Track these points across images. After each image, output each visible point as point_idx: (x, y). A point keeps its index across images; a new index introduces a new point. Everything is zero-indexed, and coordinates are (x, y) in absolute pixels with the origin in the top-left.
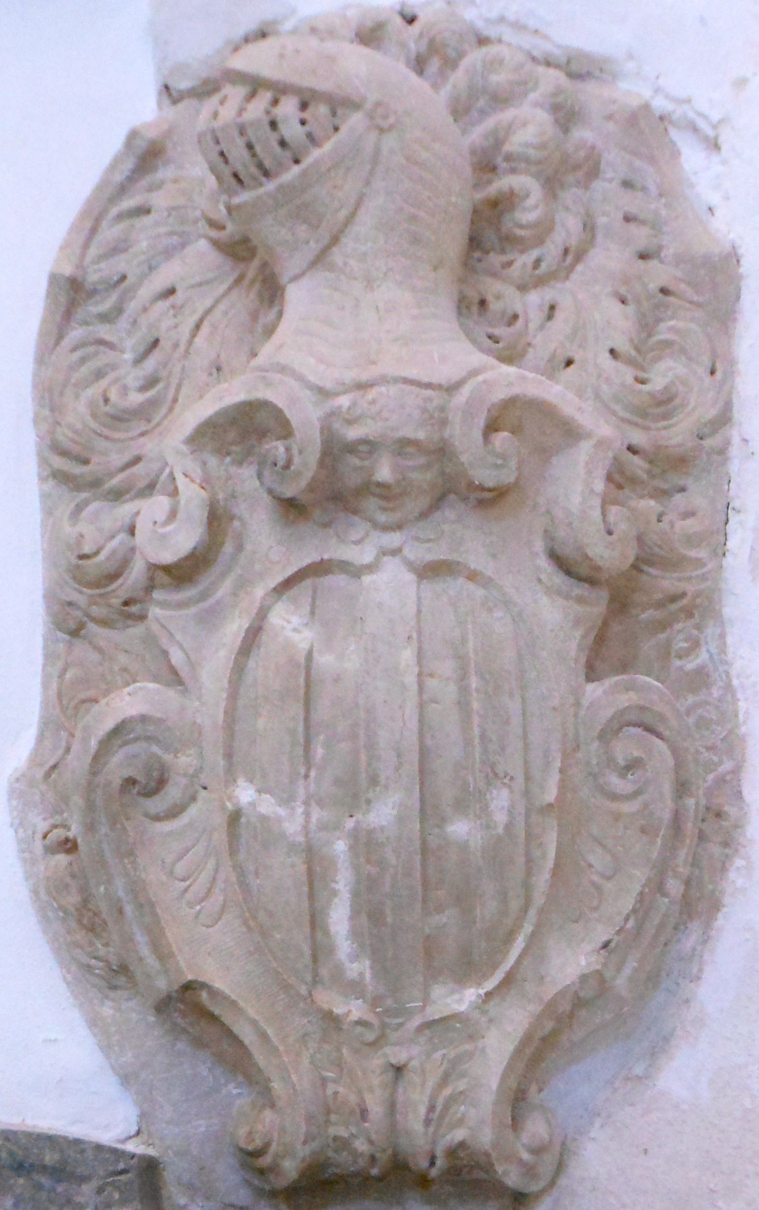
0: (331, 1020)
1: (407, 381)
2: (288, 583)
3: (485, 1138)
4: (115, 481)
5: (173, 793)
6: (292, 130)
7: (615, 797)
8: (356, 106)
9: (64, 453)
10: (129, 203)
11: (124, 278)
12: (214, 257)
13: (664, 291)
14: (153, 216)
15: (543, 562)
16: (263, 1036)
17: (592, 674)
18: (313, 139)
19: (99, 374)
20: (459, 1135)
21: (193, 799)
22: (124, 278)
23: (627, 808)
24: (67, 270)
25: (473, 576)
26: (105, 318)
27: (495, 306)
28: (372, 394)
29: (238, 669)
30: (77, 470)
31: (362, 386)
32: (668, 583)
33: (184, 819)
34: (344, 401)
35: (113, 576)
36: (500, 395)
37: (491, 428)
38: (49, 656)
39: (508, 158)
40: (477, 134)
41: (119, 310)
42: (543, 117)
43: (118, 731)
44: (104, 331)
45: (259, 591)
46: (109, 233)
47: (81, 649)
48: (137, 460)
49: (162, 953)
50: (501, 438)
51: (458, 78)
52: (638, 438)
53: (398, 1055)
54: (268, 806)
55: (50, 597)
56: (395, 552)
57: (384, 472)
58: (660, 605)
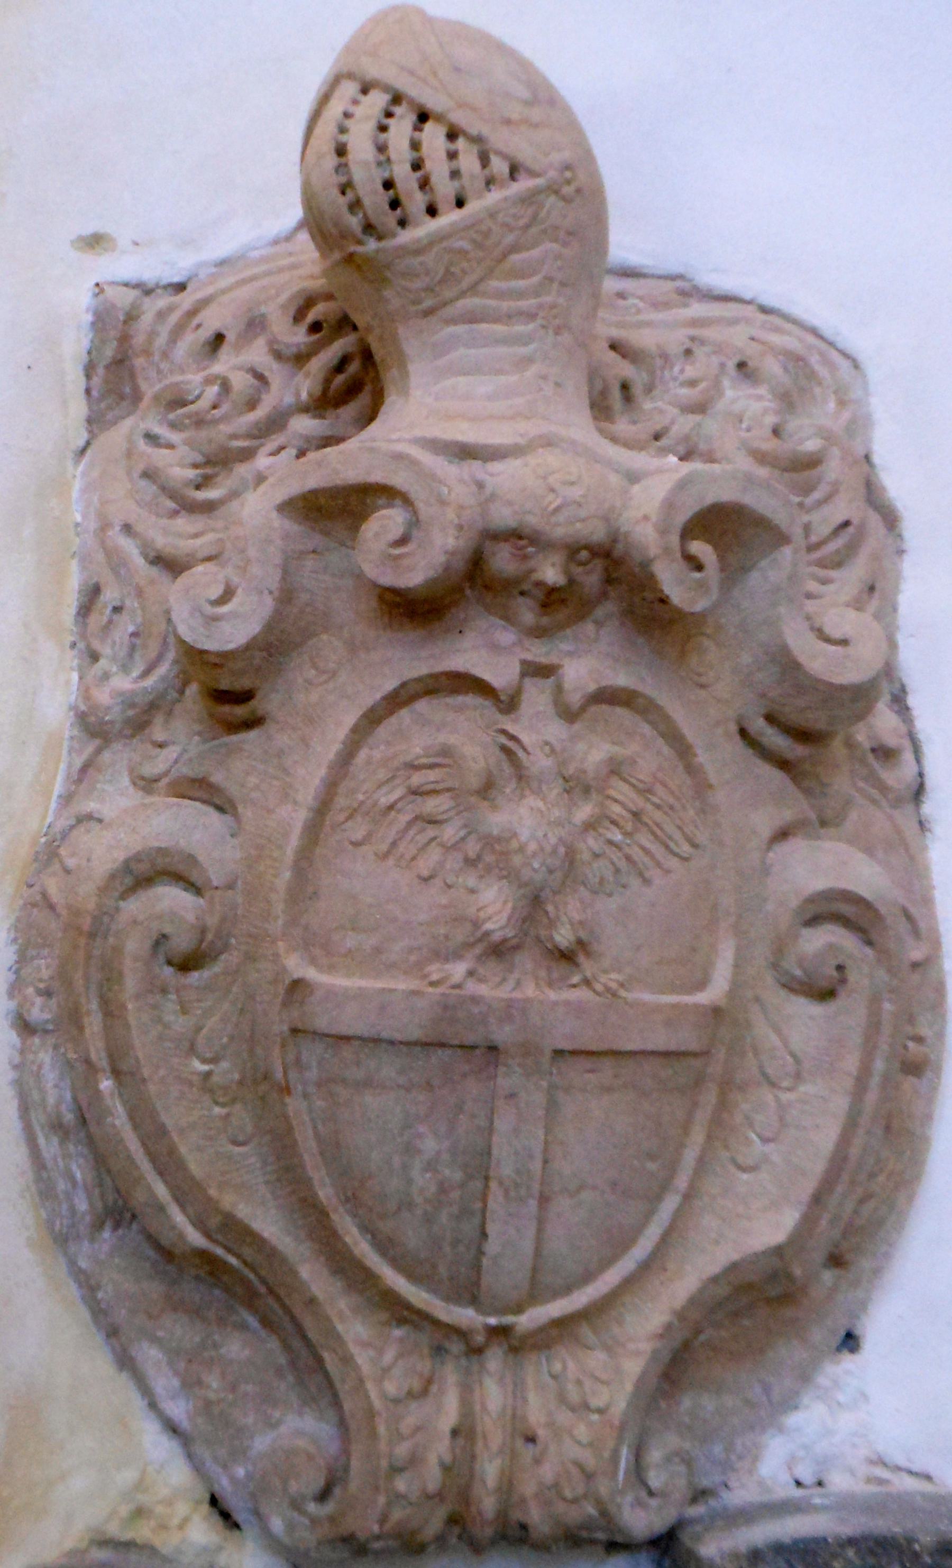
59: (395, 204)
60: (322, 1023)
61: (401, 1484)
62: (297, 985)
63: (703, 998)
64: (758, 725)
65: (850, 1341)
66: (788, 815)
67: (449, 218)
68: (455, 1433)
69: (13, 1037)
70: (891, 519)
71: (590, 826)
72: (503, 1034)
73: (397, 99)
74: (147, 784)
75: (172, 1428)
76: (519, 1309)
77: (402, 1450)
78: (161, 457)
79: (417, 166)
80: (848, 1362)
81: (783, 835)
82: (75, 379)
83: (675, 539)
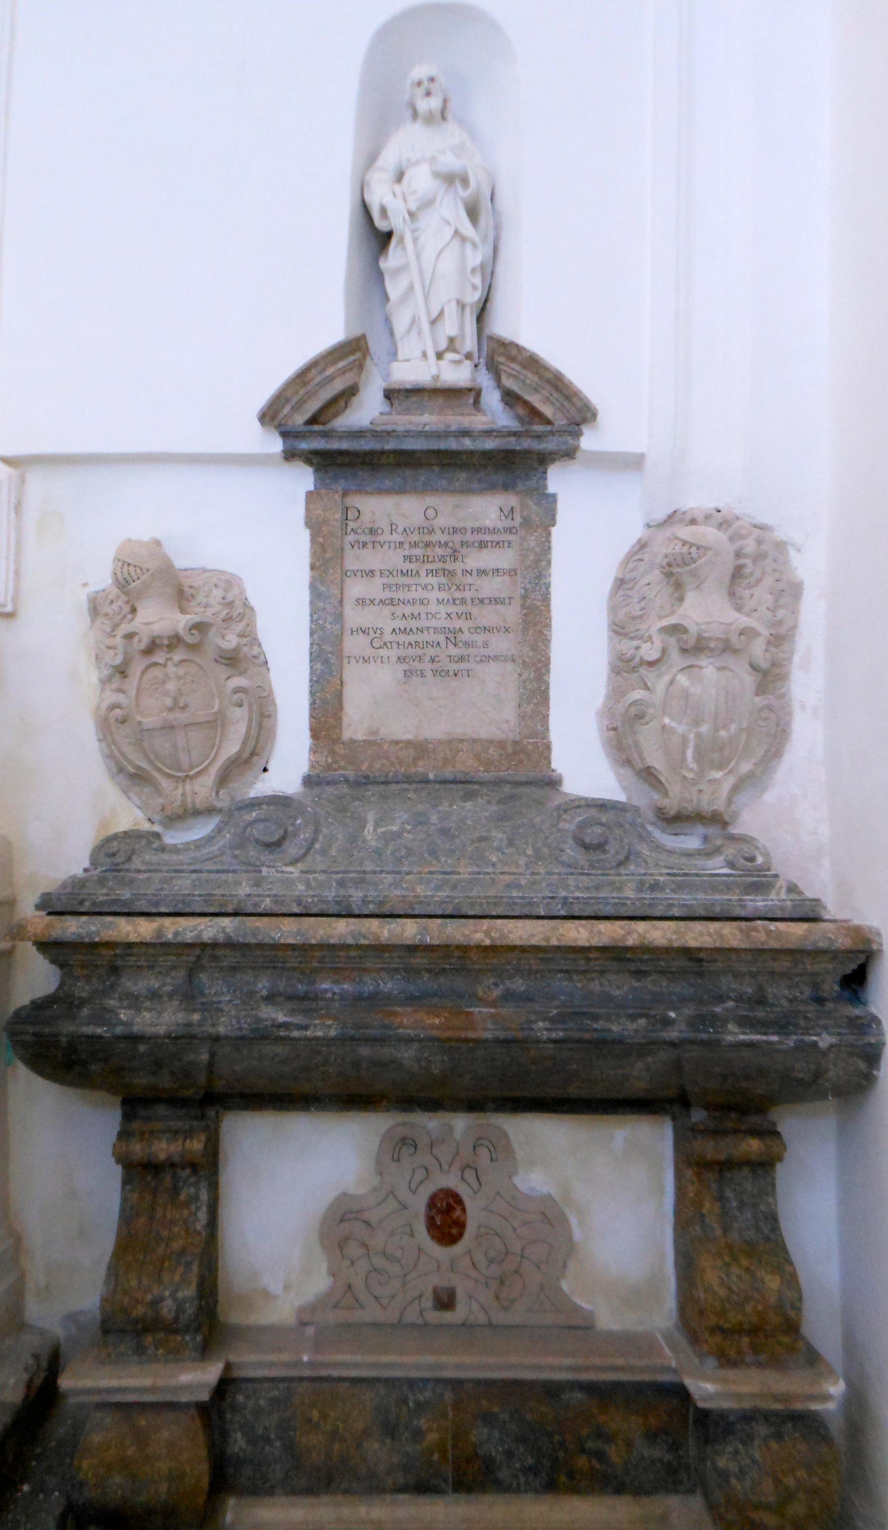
0: (685, 777)
1: (720, 623)
2: (682, 670)
3: (722, 809)
4: (632, 635)
5: (647, 718)
6: (694, 555)
7: (759, 726)
8: (710, 549)
9: (617, 625)
10: (636, 557)
11: (635, 579)
12: (661, 576)
13: (782, 591)
14: (644, 562)
15: (748, 666)
16: (668, 781)
17: (757, 695)
18: (700, 558)
19: (628, 605)
20: (715, 807)
21: (652, 720)
22: (635, 579)
23: (763, 729)
24: (621, 576)
25: (731, 670)
26: (630, 589)
27: (737, 595)
28: (711, 625)
29: (668, 688)
30: (620, 630)
31: (709, 623)
32: (777, 671)
33: (648, 726)
34: (703, 627)
35: (631, 660)
36: (743, 626)
37: (740, 634)
38: (609, 679)
39: (744, 554)
40: (737, 545)
41: (633, 587)
42: (754, 543)
43: (634, 702)
44: (628, 592)
45: (674, 670)
46: (631, 565)
47: (619, 678)
48: (638, 630)
49: (642, 759)
50: (742, 637)
51: (731, 531)
52: (773, 632)
53: (701, 787)
54: (673, 724)
55: (610, 663)
56: (712, 663)
57: (712, 645)
58: (775, 676)
59: (127, 582)
60: (145, 728)
61: (174, 805)
62: (140, 722)
63: (213, 711)
64: (219, 659)
65: (265, 770)
66: (229, 674)
67: (137, 582)
68: (182, 795)
69: (98, 743)
70: (252, 609)
71: (183, 685)
72: (174, 723)
73: (124, 562)
74: (113, 691)
75: (139, 808)
76: (190, 771)
77: (173, 799)
78: (105, 627)
79: (129, 574)
80: (266, 774)
81: (229, 678)
82: (87, 614)
83: (188, 632)
